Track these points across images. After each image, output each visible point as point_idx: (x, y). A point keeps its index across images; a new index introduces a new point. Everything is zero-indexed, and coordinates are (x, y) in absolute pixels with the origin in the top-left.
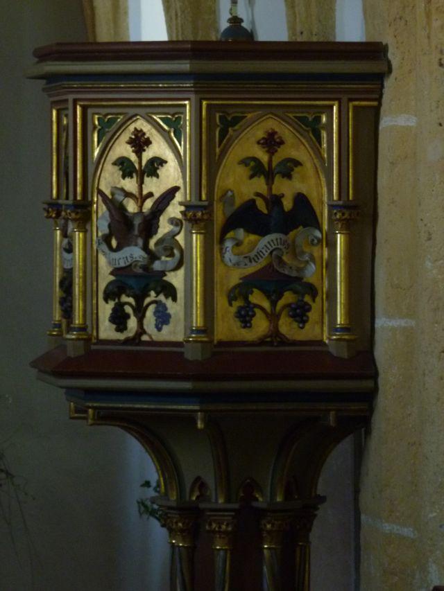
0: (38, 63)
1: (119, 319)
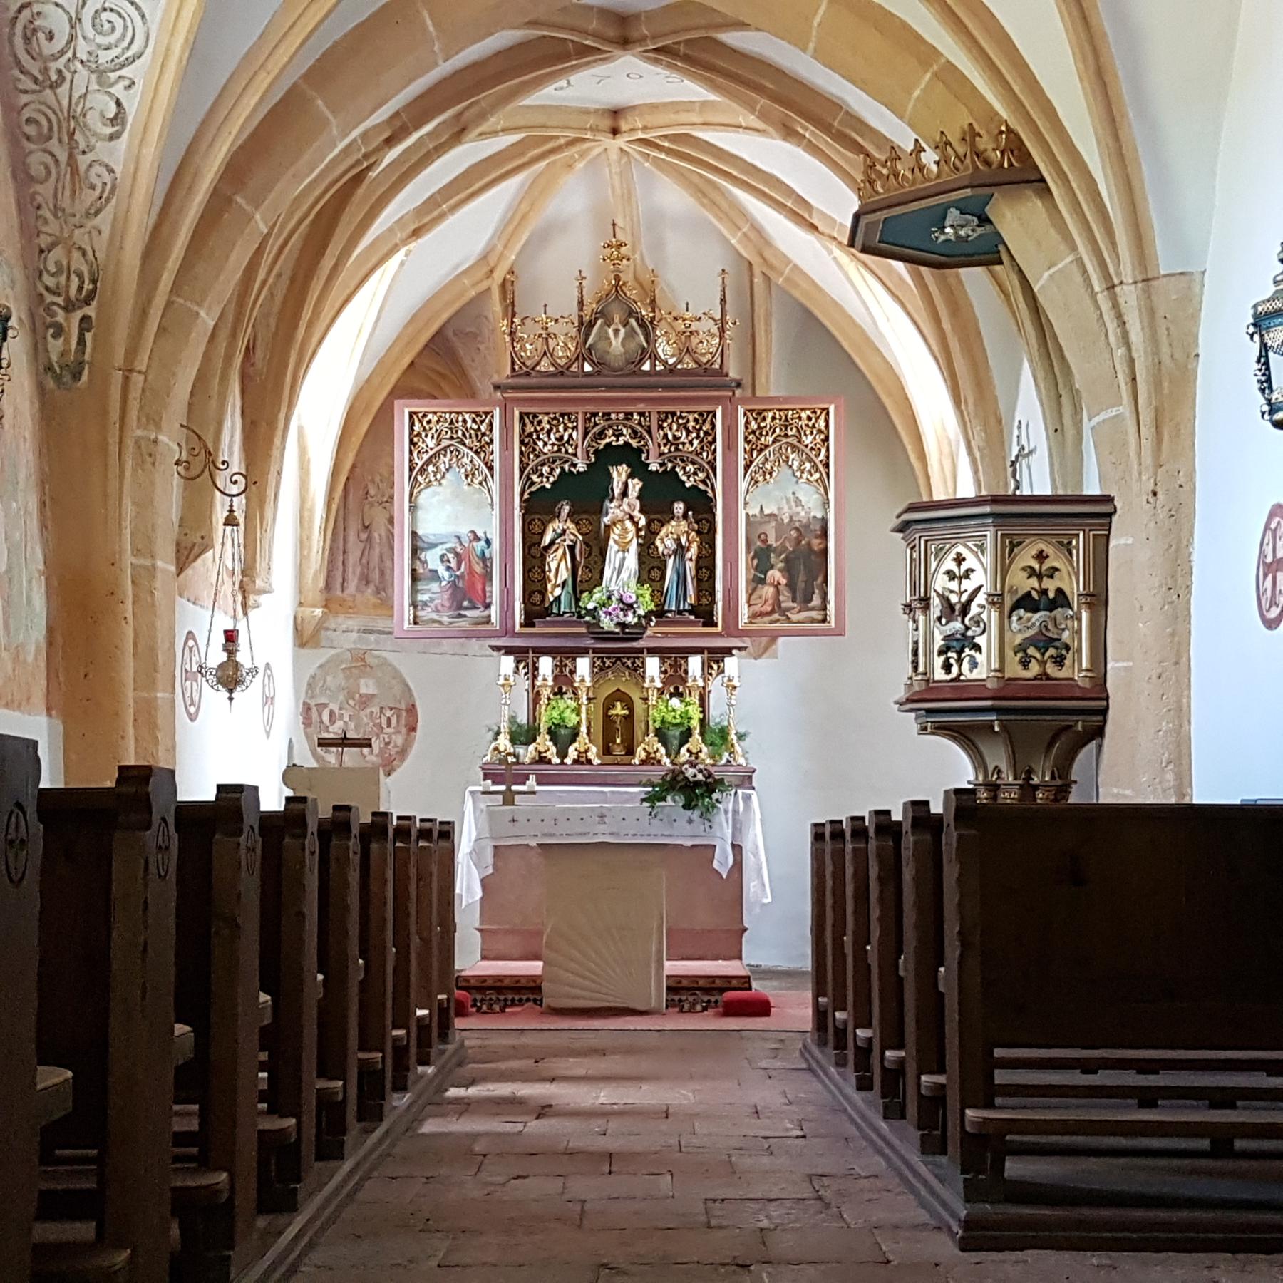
0: (1050, 716)
1: (947, 667)
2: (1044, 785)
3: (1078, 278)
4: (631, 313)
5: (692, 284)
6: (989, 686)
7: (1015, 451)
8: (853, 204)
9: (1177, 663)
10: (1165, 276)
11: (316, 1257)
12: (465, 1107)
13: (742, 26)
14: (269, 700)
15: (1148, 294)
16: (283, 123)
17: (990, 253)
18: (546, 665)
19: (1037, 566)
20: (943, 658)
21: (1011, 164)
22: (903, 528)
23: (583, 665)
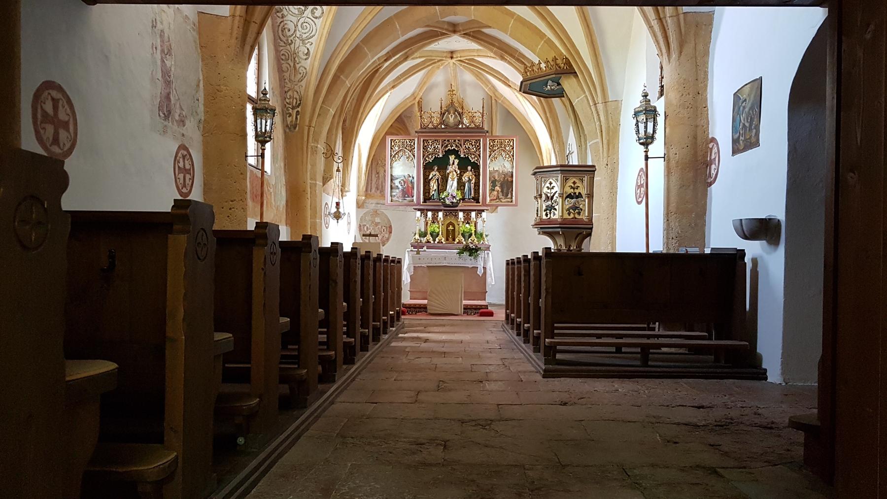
0: (577, 229)
1: (547, 215)
4: (456, 110)
5: (474, 102)
8: (521, 79)
11: (359, 377)
12: (404, 339)
13: (490, 27)
14: (349, 223)
15: (606, 106)
16: (355, 55)
17: (561, 94)
18: (430, 214)
22: (534, 174)
23: (441, 214)
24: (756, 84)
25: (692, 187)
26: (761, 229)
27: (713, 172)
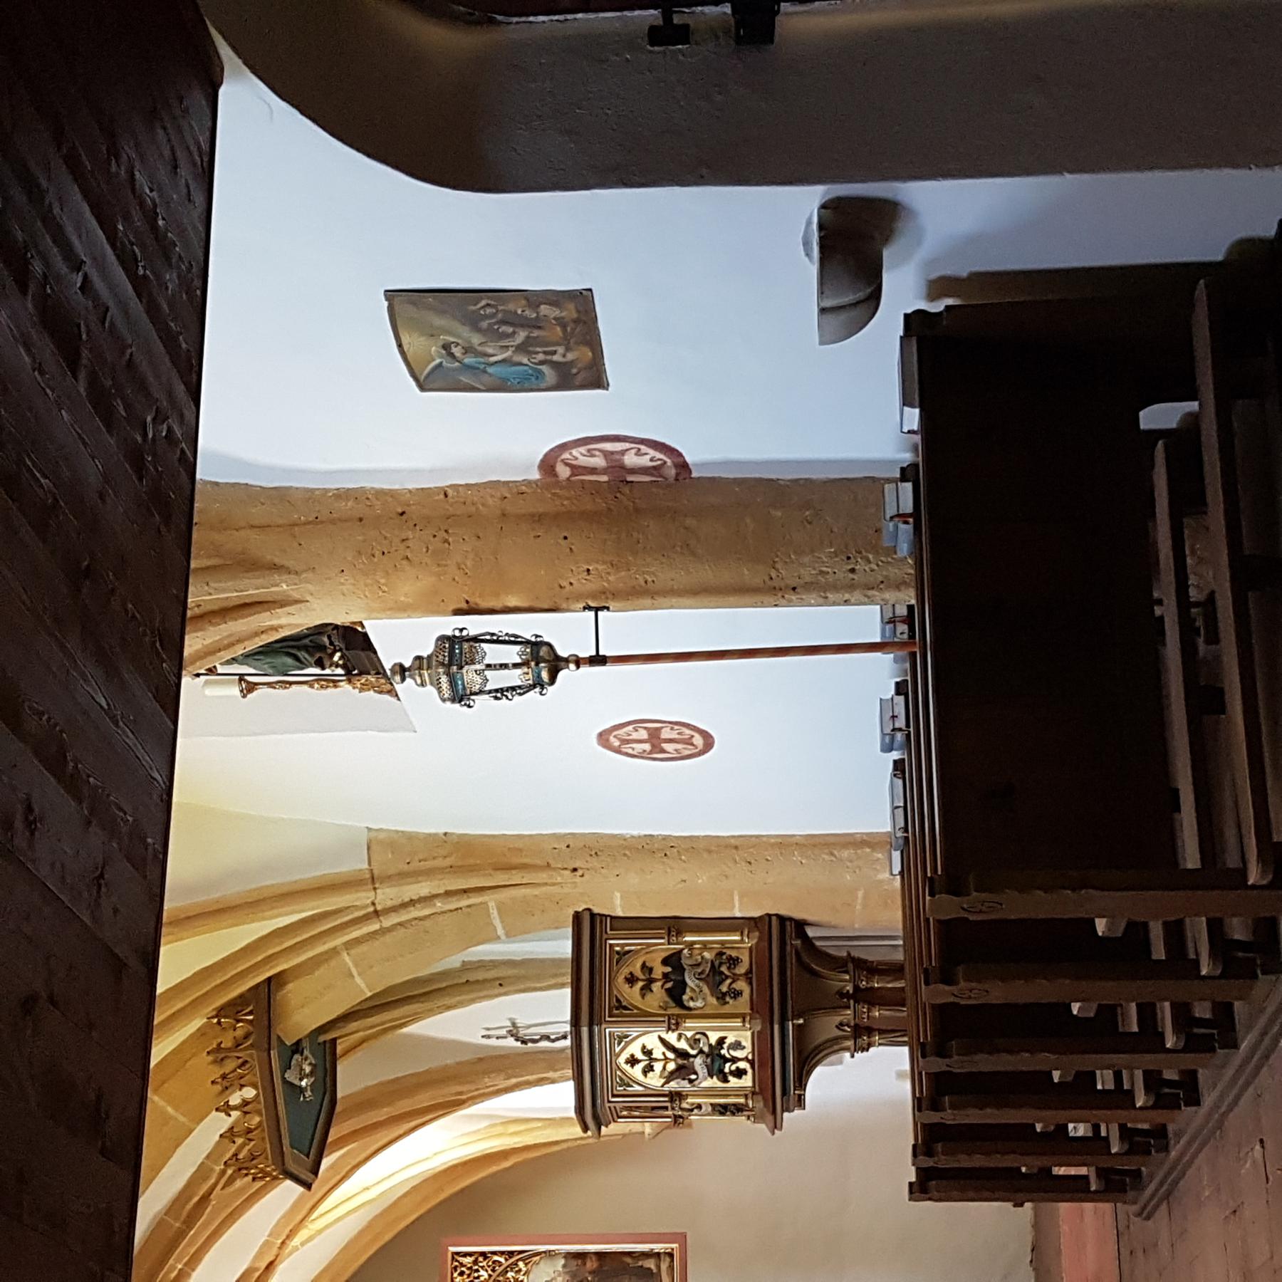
1: (740, 1073)
2: (853, 980)
3: (364, 948)
6: (758, 1028)
7: (511, 1042)
9: (736, 848)
10: (370, 864)
15: (388, 879)
17: (324, 1049)
19: (640, 984)
20: (730, 1078)
21: (250, 1013)
24: (404, 309)
25: (689, 522)
26: (851, 250)
27: (647, 458)
